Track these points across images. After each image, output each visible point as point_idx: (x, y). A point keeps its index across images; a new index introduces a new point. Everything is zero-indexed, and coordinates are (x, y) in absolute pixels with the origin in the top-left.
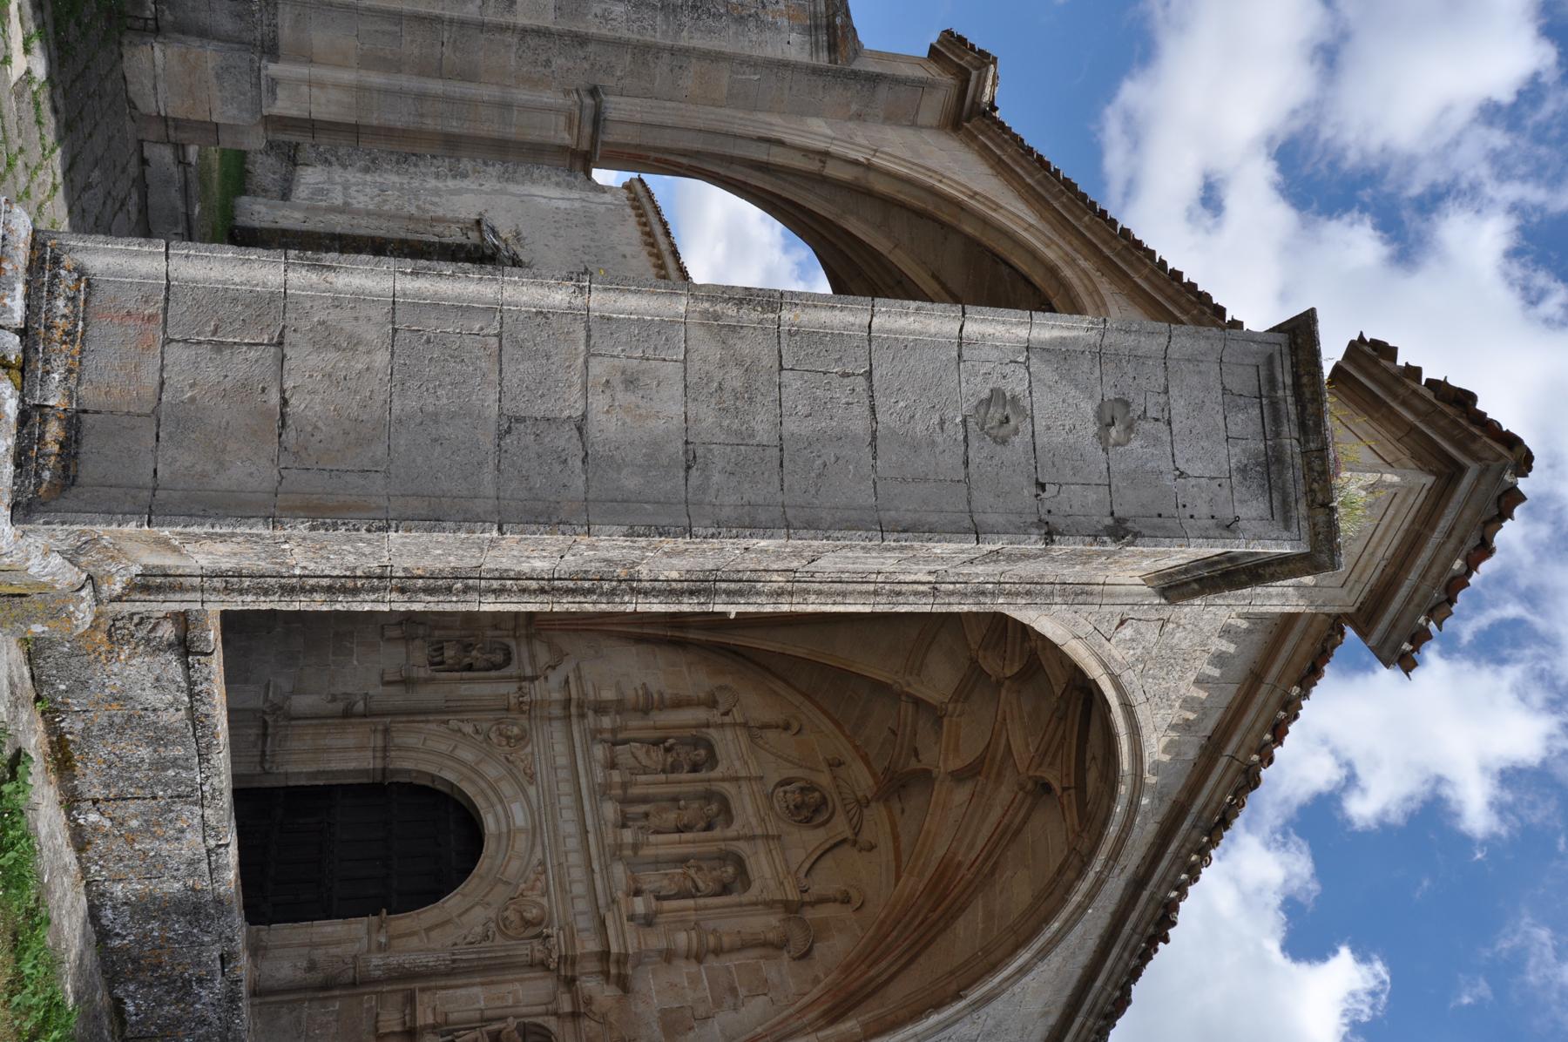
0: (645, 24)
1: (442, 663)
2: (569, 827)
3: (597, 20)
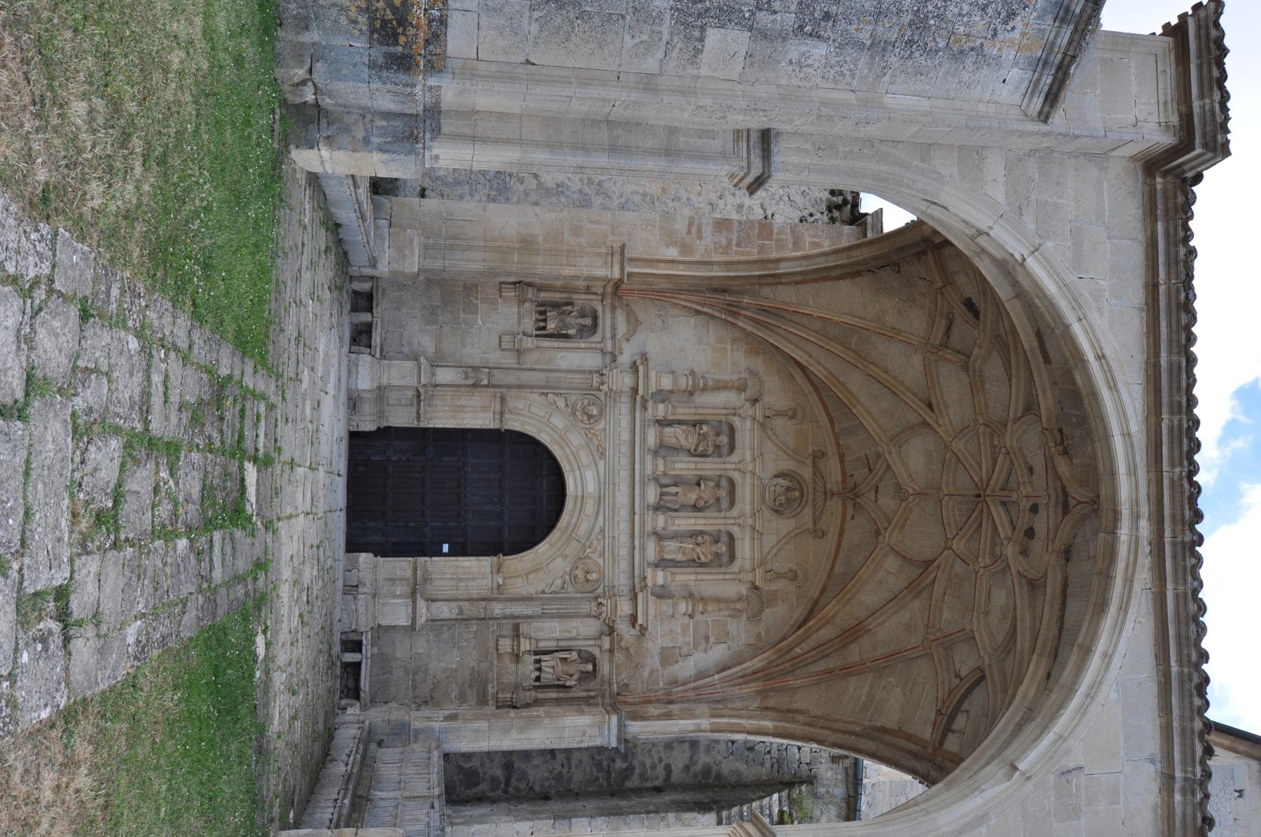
1: (544, 328)
3: (791, 68)
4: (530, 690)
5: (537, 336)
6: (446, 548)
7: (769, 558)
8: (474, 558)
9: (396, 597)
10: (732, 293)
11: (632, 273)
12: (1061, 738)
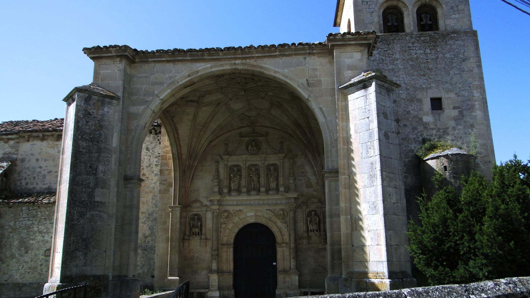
0: (105, 160)
3: (106, 175)
4: (320, 234)
6: (274, 264)
12: (299, 86)
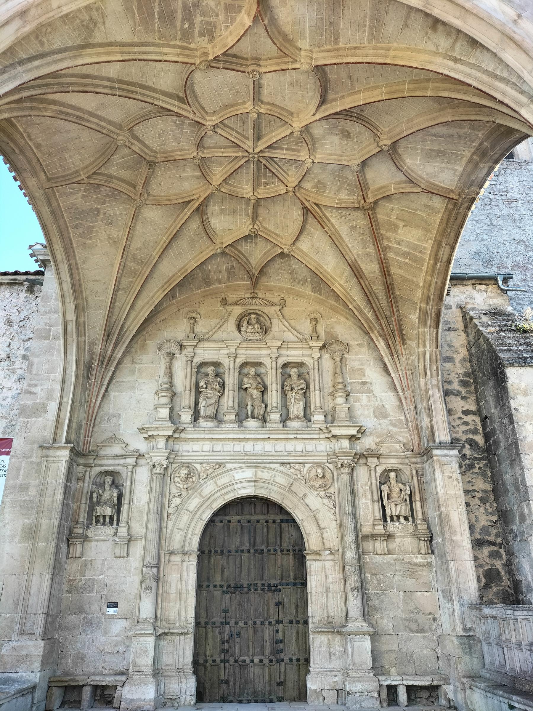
1: (111, 517)
2: (259, 447)
4: (416, 525)
5: (118, 524)
7: (301, 337)
8: (308, 577)
9: (345, 650)
10: (91, 361)
11: (66, 440)
